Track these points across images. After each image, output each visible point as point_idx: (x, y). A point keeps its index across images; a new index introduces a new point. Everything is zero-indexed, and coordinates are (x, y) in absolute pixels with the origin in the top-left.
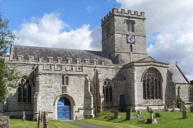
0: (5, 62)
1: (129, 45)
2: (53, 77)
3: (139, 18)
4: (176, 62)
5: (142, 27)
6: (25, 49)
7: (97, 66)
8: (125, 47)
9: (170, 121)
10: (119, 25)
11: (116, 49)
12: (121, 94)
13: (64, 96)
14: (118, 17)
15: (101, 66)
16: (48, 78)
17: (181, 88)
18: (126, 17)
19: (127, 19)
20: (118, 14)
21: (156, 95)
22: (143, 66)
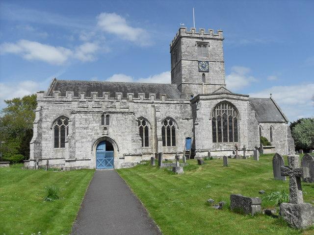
0: (37, 99)
1: (201, 73)
2: (90, 116)
3: (215, 39)
4: (271, 95)
5: (219, 49)
6: (70, 84)
7: (155, 102)
8: (195, 77)
9: (6, 201)
10: (188, 50)
11: (183, 80)
12: (187, 136)
13: (104, 139)
14: (186, 39)
15: (160, 102)
16: (84, 117)
17: (276, 128)
18: (198, 38)
19: (199, 40)
20: (186, 35)
21: (225, 136)
22: (212, 99)
